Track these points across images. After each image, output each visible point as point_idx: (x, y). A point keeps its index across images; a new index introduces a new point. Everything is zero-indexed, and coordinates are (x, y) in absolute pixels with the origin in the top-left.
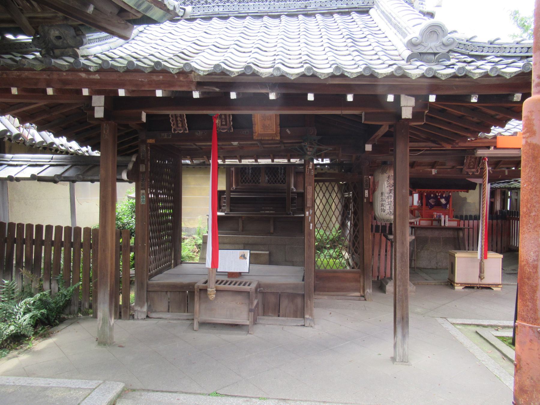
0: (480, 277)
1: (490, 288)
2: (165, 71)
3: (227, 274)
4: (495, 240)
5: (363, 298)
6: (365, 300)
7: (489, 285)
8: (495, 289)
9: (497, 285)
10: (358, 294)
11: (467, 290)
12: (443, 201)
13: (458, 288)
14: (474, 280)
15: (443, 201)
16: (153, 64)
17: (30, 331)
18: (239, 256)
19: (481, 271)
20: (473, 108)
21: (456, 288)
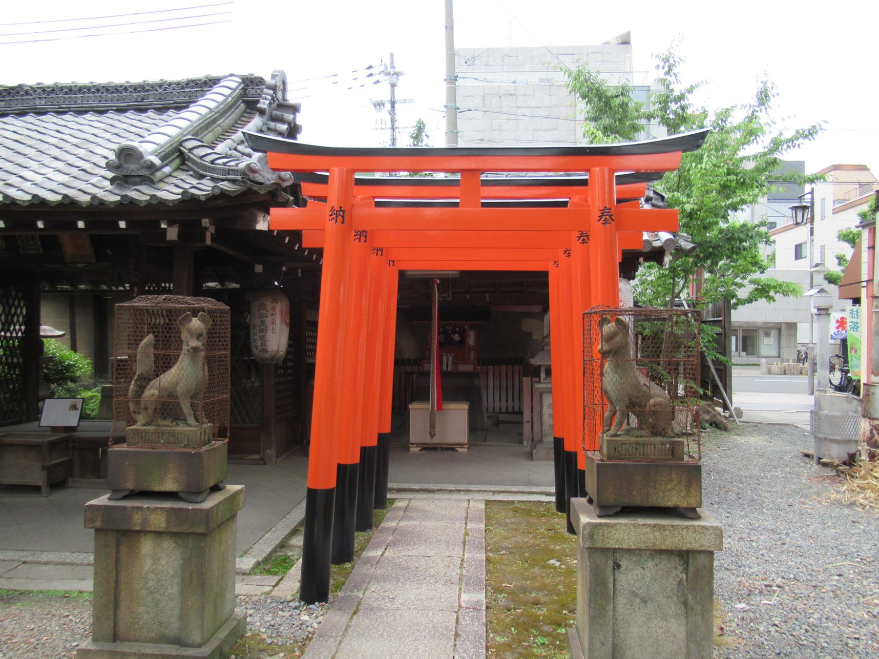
0: (432, 435)
1: (453, 449)
2: (43, 202)
3: (49, 429)
4: (504, 384)
5: (261, 462)
6: (265, 464)
7: (452, 444)
8: (460, 450)
9: (461, 445)
10: (257, 457)
11: (424, 452)
12: (456, 337)
13: (415, 450)
14: (428, 440)
15: (456, 337)
16: (180, 196)
17: (587, 497)
18: (68, 407)
19: (432, 426)
20: (123, 236)
21: (411, 449)
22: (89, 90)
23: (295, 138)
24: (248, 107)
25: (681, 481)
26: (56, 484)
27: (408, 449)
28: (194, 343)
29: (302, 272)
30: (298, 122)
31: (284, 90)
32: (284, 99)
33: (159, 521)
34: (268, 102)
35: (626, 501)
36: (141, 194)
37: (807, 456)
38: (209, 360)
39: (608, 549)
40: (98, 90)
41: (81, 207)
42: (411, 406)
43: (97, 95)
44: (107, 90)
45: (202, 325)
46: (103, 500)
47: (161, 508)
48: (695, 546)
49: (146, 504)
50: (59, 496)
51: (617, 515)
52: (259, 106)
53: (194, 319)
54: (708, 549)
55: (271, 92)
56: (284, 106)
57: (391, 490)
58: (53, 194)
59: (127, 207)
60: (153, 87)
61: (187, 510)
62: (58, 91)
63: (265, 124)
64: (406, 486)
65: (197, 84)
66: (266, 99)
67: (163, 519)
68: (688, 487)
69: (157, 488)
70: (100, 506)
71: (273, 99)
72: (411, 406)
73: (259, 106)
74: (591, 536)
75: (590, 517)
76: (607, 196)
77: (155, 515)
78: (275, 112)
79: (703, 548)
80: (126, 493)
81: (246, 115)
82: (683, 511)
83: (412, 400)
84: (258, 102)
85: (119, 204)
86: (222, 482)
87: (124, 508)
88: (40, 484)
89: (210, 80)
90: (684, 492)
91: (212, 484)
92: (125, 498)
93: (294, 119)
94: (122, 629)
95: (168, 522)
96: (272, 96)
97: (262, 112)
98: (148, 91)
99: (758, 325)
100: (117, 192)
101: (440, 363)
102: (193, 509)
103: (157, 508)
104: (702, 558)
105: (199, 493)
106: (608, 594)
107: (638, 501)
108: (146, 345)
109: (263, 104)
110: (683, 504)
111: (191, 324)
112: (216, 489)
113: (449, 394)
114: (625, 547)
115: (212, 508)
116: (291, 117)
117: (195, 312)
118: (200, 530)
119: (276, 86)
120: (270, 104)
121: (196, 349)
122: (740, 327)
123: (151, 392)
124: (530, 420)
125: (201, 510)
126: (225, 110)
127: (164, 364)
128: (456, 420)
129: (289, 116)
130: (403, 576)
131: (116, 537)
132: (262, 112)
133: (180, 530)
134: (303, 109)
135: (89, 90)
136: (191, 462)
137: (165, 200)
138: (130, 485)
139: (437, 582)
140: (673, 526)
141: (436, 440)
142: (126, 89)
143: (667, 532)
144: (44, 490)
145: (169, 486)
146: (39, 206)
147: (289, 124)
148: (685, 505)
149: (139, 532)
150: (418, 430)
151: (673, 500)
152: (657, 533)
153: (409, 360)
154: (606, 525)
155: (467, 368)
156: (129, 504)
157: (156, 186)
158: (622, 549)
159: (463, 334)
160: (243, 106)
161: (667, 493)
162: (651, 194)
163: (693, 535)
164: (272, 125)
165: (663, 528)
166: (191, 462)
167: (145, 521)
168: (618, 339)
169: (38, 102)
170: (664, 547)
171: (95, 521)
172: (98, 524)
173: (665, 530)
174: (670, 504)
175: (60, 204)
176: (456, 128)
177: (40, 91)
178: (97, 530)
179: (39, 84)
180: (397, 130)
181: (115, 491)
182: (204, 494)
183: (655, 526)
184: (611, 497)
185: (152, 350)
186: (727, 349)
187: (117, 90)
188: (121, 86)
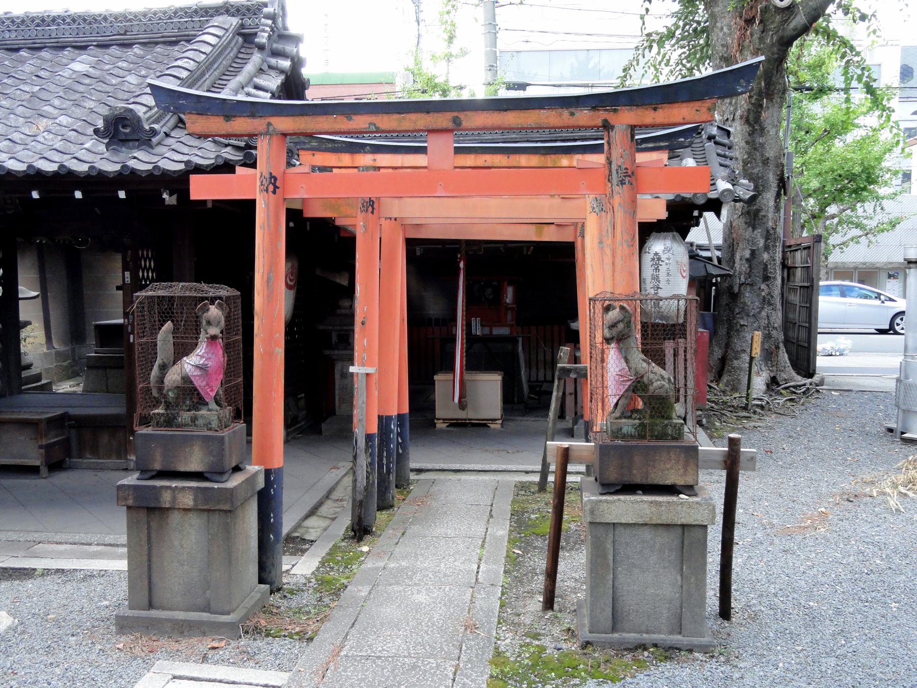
1: (485, 425)
2: (39, 173)
14: (461, 415)
21: (437, 425)
22: (64, 20)
23: (302, 97)
24: (245, 41)
25: (679, 460)
26: (56, 466)
27: (434, 425)
28: (214, 331)
29: (311, 225)
30: (302, 55)
31: (284, 16)
32: (285, 28)
33: (187, 500)
34: (266, 35)
35: (627, 479)
36: (141, 161)
37: (891, 430)
38: (228, 347)
39: (609, 524)
40: (74, 21)
41: (78, 177)
42: (436, 377)
43: (74, 26)
44: (85, 20)
45: (220, 313)
46: (131, 479)
47: (188, 488)
48: (691, 521)
49: (174, 484)
50: (62, 479)
51: (617, 492)
52: (257, 40)
53: (212, 308)
54: (701, 523)
55: (270, 22)
56: (284, 37)
57: (570, 473)
58: (48, 163)
59: (128, 178)
60: (135, 16)
61: (213, 488)
62: (28, 22)
63: (264, 61)
64: (466, 467)
65: (186, 13)
66: (264, 31)
67: (191, 497)
68: (685, 467)
69: (182, 468)
70: (129, 486)
71: (272, 30)
72: (436, 377)
73: (257, 40)
74: (592, 512)
75: (593, 494)
76: (651, 145)
77: (183, 493)
78: (275, 46)
79: (697, 523)
80: (154, 473)
81: (241, 56)
82: (680, 489)
83: (435, 373)
84: (255, 34)
85: (119, 174)
86: (242, 462)
87: (154, 487)
88: (38, 463)
89: (201, 9)
90: (682, 471)
91: (234, 465)
92: (152, 478)
93: (297, 52)
94: (156, 601)
95: (195, 500)
96: (271, 27)
97: (261, 48)
98: (130, 20)
99: (878, 265)
100: (115, 159)
101: (468, 326)
102: (218, 488)
103: (184, 488)
104: (697, 533)
105: (222, 473)
106: (608, 565)
107: (638, 479)
108: (166, 332)
109: (262, 38)
110: (680, 481)
111: (210, 313)
112: (237, 469)
113: (475, 364)
114: (623, 521)
115: (235, 487)
116: (295, 50)
117: (212, 300)
118: (226, 507)
119: (275, 14)
120: (269, 36)
121: (214, 338)
122: (856, 268)
123: (173, 377)
124: (573, 391)
125: (226, 489)
126: (220, 51)
127: (183, 349)
128: (489, 389)
129: (290, 48)
130: (422, 555)
131: (147, 511)
132: (261, 48)
133: (205, 507)
134: (306, 39)
135: (64, 20)
136: (214, 444)
137: (168, 170)
138: (157, 466)
139: (455, 561)
140: (669, 502)
141: (469, 414)
142: (105, 19)
143: (663, 508)
144: (44, 470)
145: (195, 464)
146: (35, 178)
147: (292, 60)
148: (682, 483)
149: (168, 509)
150: (446, 406)
151: (672, 478)
152: (653, 509)
153: (437, 320)
154: (607, 502)
155: (504, 331)
156: (159, 483)
157: (154, 151)
158: (621, 524)
159: (499, 294)
160: (240, 39)
161: (666, 472)
162: (714, 131)
163: (688, 511)
164: (273, 61)
165: (659, 504)
166: (214, 444)
167: (174, 499)
168: (621, 326)
169: (7, 35)
170: (659, 522)
171: (126, 499)
172: (130, 502)
173: (661, 506)
174: (668, 482)
175: (56, 174)
176: (494, 21)
177: (8, 22)
178: (129, 508)
179: (6, 13)
180: (422, 24)
181: (143, 471)
182: (227, 475)
183: (651, 502)
184: (613, 475)
185: (171, 336)
186: (813, 305)
187: (96, 20)
188: (100, 15)
